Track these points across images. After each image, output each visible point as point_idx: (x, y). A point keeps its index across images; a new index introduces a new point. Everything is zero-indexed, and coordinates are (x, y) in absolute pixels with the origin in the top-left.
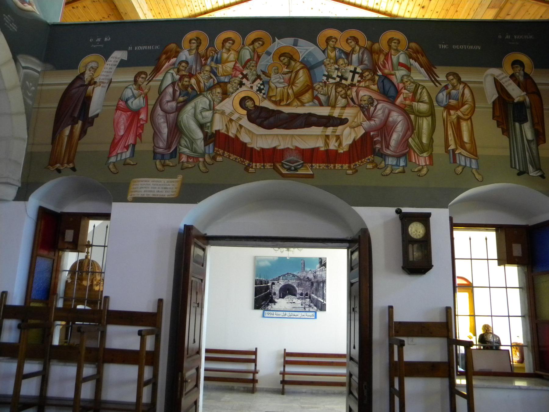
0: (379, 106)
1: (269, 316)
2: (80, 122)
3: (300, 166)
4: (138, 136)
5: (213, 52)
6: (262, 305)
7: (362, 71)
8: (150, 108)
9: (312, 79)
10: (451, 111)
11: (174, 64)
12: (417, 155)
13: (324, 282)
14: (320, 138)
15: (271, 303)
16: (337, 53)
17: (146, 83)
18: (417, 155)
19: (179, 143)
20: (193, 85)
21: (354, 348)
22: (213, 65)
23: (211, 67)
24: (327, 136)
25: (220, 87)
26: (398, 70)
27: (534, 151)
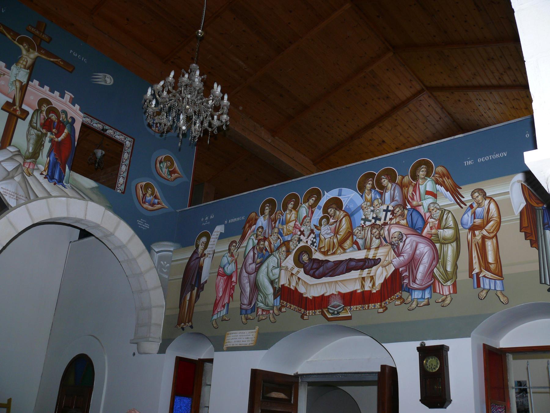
3: (342, 309)
4: (231, 296)
5: (280, 215)
7: (393, 208)
8: (239, 270)
10: (475, 231)
11: (254, 231)
12: (442, 284)
16: (372, 194)
17: (236, 250)
18: (442, 284)
20: (266, 247)
22: (280, 227)
24: (363, 278)
26: (425, 199)
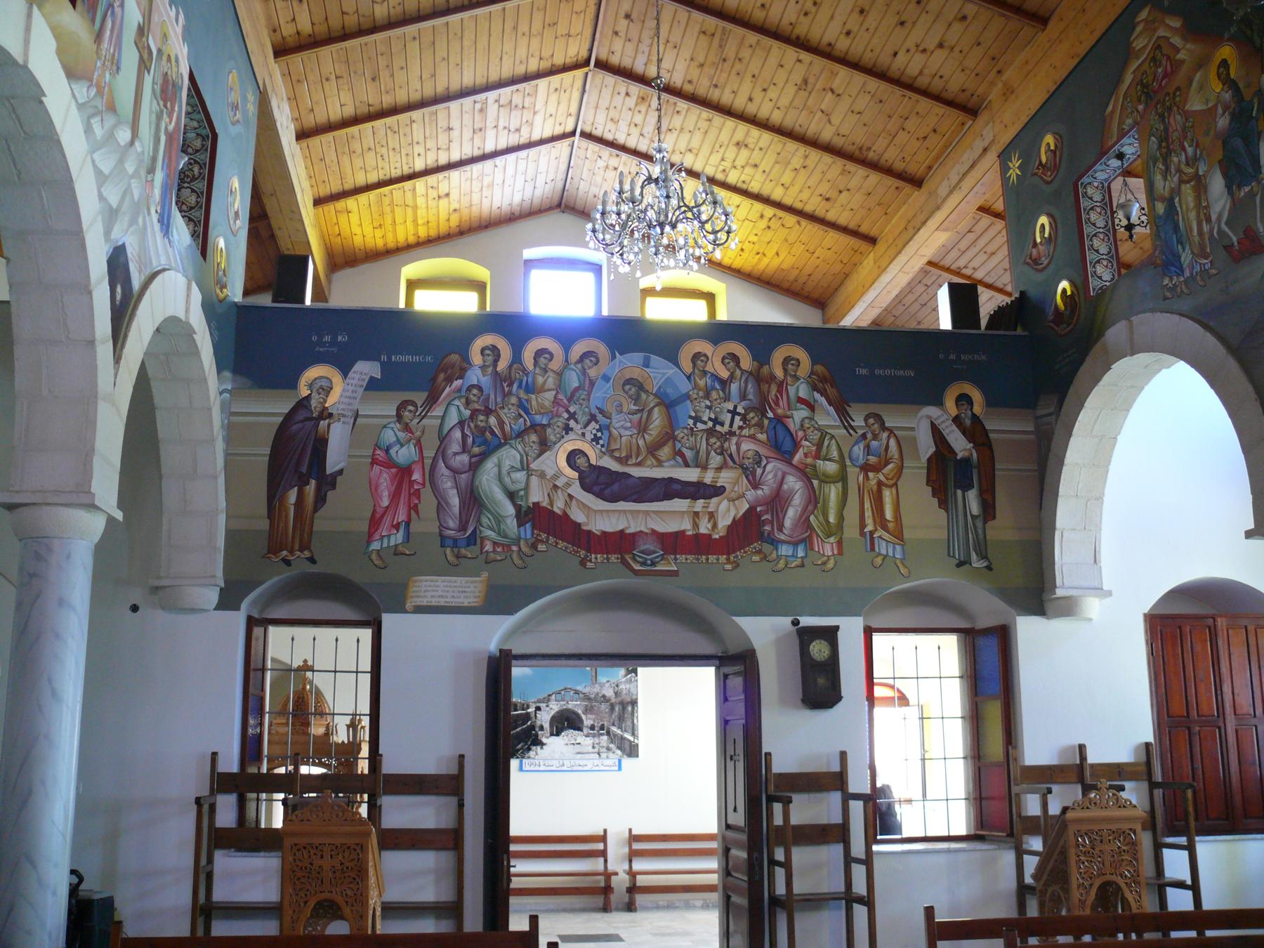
0: (769, 467)
1: (532, 768)
2: (313, 482)
6: (519, 750)
8: (428, 462)
9: (671, 422)
11: (459, 390)
13: (634, 703)
14: (686, 516)
15: (534, 745)
19: (479, 521)
21: (735, 810)
23: (520, 399)
24: (696, 514)
25: (536, 432)
26: (796, 409)
27: (980, 532)
